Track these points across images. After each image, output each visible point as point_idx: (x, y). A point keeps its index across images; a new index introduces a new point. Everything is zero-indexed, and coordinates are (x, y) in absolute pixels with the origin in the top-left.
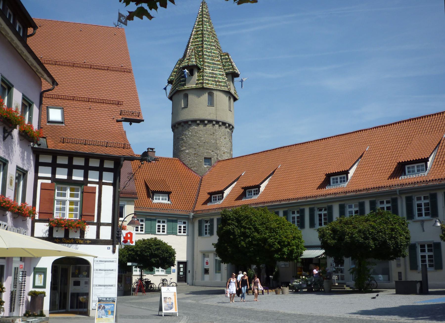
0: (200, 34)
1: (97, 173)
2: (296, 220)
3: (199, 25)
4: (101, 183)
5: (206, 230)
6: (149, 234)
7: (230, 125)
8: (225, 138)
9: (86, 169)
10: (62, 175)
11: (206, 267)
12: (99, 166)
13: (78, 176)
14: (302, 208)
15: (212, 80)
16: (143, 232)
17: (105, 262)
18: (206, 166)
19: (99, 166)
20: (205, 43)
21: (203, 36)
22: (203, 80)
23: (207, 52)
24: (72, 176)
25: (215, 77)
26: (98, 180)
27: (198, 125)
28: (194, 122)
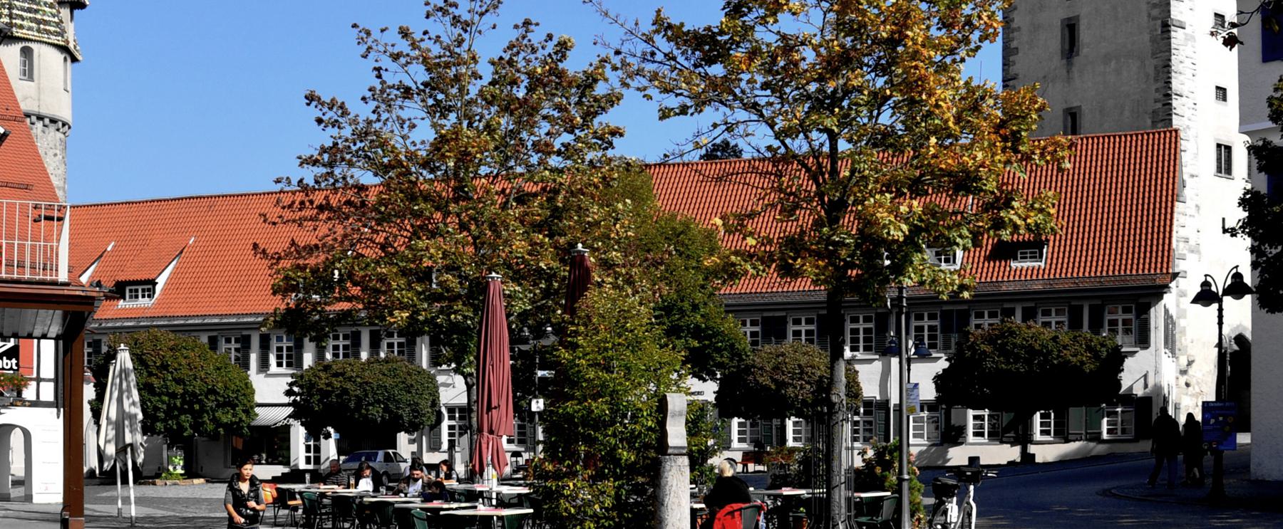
8: (55, 155)
14: (245, 333)
15: (30, 18)
25: (36, 11)
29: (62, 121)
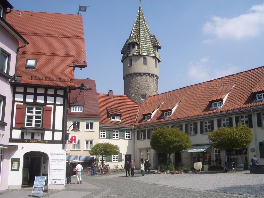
0: (138, 25)
1: (53, 98)
2: (192, 129)
3: (138, 20)
4: (55, 105)
5: (142, 136)
6: (108, 139)
7: (156, 76)
9: (46, 95)
10: (30, 99)
11: (142, 158)
12: (54, 94)
13: (40, 100)
14: (196, 122)
16: (105, 138)
17: (58, 154)
18: (142, 100)
19: (54, 94)
20: (141, 30)
21: (140, 26)
22: (140, 50)
23: (142, 34)
24: (36, 100)
25: (147, 49)
26: (53, 103)
27: (138, 76)
28: (135, 74)
29: (155, 75)
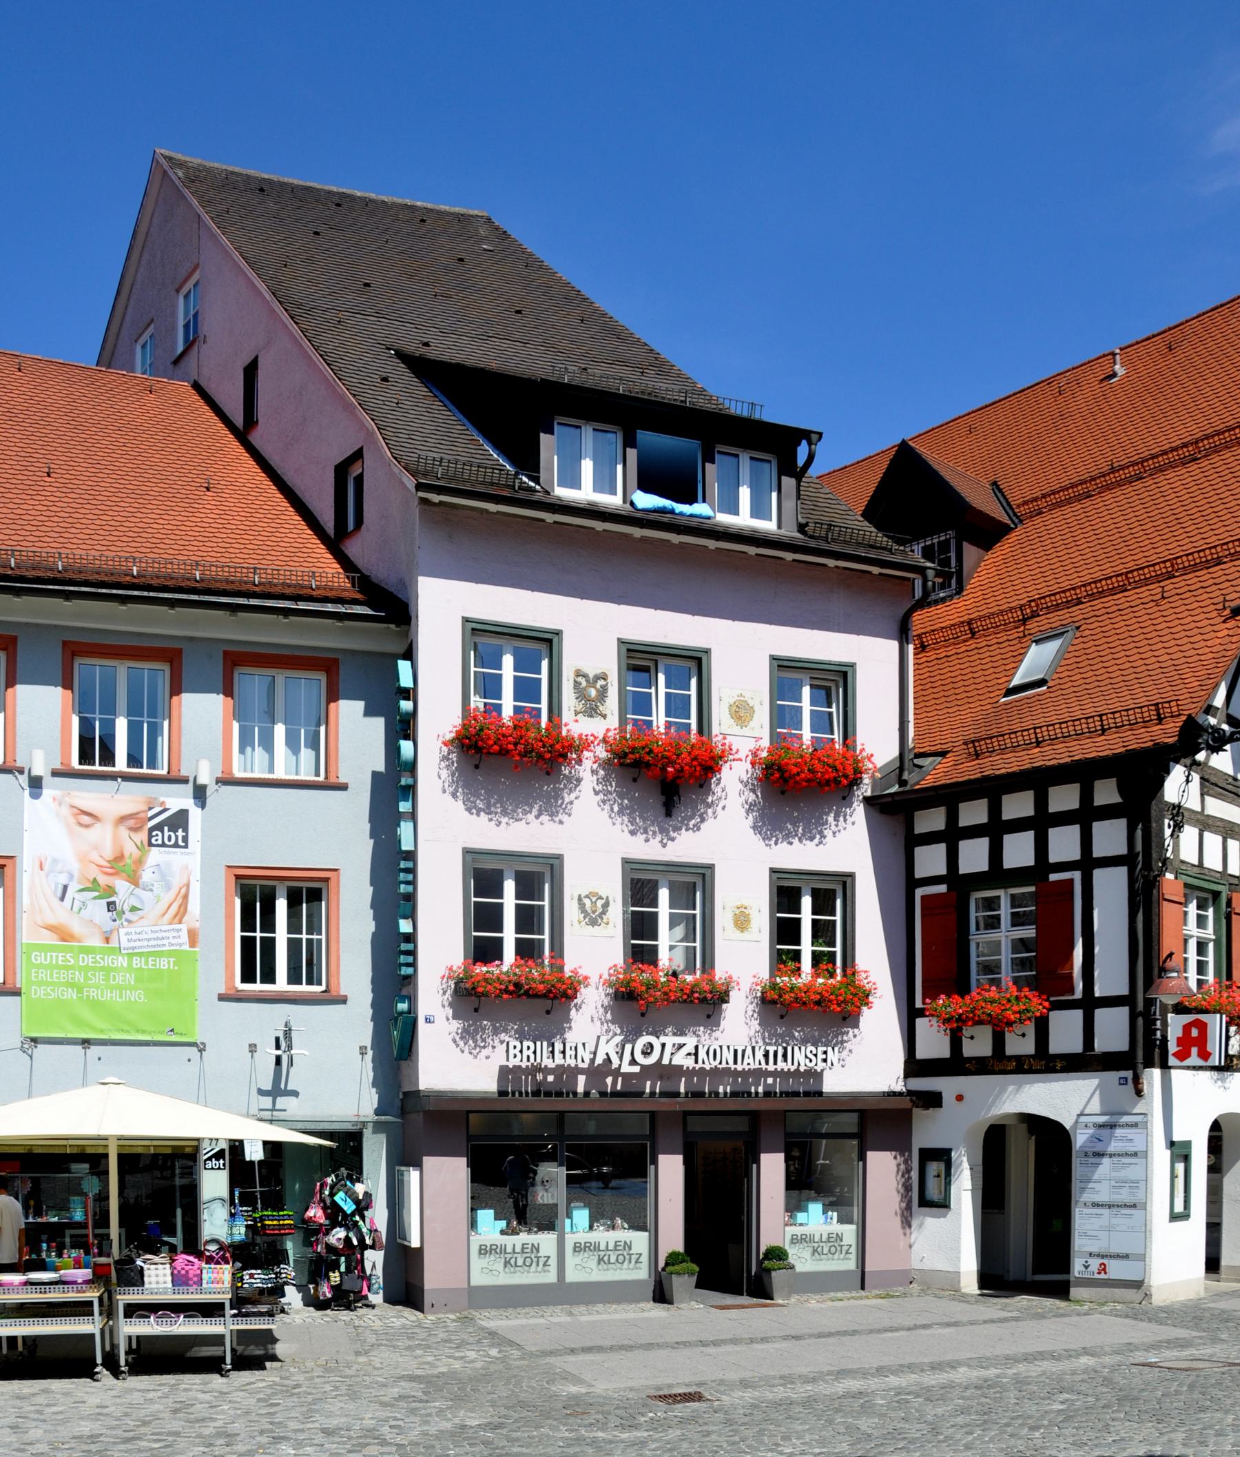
12: (1032, 813)
19: (1032, 813)
